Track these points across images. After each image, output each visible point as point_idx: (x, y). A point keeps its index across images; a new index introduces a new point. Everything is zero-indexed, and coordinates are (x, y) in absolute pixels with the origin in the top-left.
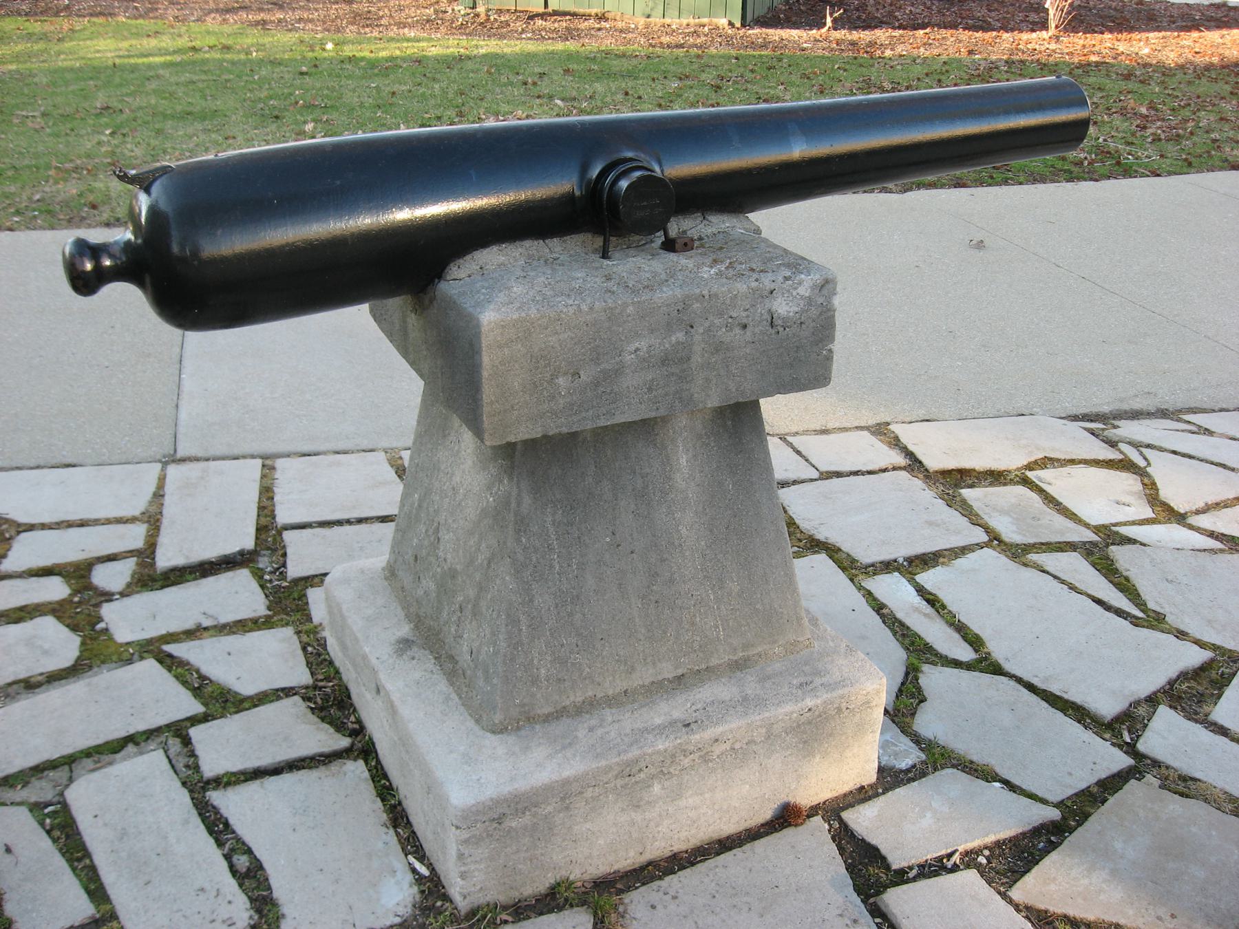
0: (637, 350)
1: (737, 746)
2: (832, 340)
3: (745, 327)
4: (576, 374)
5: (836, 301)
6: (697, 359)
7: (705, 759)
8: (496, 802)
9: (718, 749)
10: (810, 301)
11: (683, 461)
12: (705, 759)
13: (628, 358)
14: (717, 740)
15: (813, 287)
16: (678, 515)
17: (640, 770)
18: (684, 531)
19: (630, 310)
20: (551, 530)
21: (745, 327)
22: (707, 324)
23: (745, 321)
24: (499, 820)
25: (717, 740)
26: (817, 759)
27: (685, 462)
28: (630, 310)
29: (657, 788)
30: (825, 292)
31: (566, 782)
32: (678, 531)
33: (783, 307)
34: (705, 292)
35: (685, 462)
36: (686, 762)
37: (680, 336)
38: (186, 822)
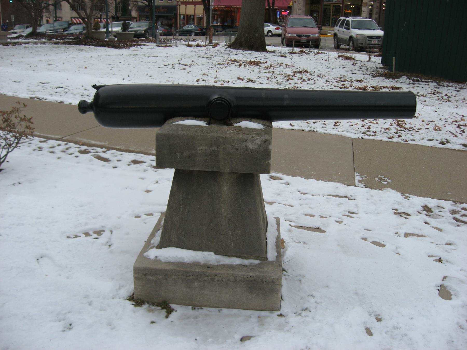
0: (201, 149)
1: (224, 280)
2: (270, 159)
3: (237, 149)
4: (182, 153)
5: (271, 147)
6: (221, 156)
7: (212, 280)
8: (145, 269)
9: (217, 278)
10: (260, 145)
11: (226, 188)
12: (212, 280)
13: (199, 152)
14: (216, 275)
15: (262, 141)
16: (222, 205)
17: (190, 276)
18: (223, 211)
19: (199, 137)
20: (181, 198)
21: (237, 149)
22: (224, 146)
23: (237, 147)
24: (145, 275)
25: (216, 275)
26: (254, 295)
27: (226, 189)
28: (199, 137)
29: (196, 284)
30: (266, 143)
31: (166, 271)
32: (221, 210)
33: (250, 146)
34: (224, 137)
35: (226, 189)
36: (206, 278)
37: (215, 148)
38: (131, 271)
